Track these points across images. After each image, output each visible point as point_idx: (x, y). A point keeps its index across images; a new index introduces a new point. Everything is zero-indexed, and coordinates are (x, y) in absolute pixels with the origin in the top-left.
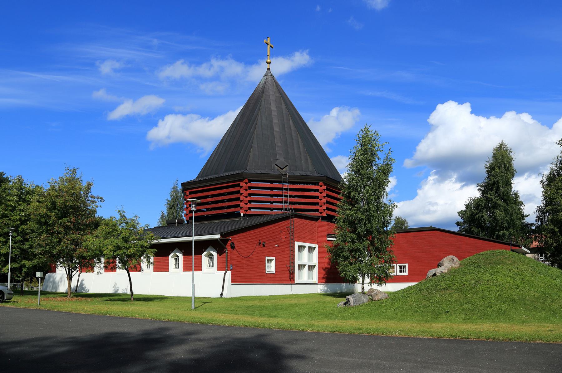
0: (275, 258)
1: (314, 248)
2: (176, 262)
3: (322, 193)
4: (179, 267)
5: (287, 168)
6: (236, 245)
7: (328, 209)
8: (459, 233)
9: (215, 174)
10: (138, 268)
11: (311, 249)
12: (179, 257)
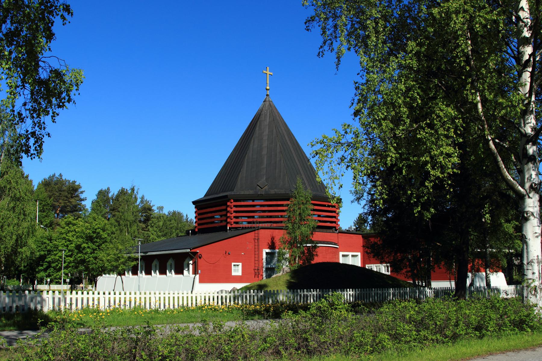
1: (357, 256)
10: (124, 274)
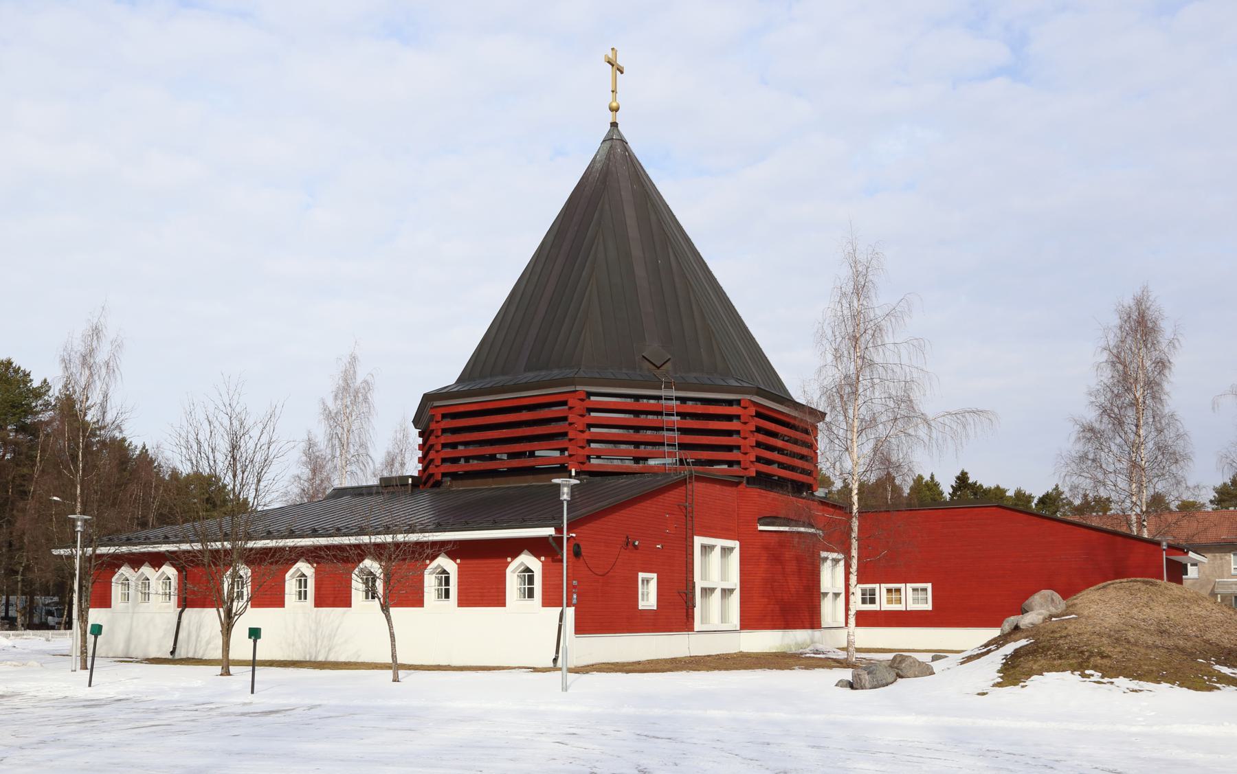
0: (655, 575)
1: (731, 549)
2: (300, 587)
4: (305, 598)
5: (669, 365)
6: (583, 550)
7: (759, 459)
8: (1012, 507)
11: (726, 551)
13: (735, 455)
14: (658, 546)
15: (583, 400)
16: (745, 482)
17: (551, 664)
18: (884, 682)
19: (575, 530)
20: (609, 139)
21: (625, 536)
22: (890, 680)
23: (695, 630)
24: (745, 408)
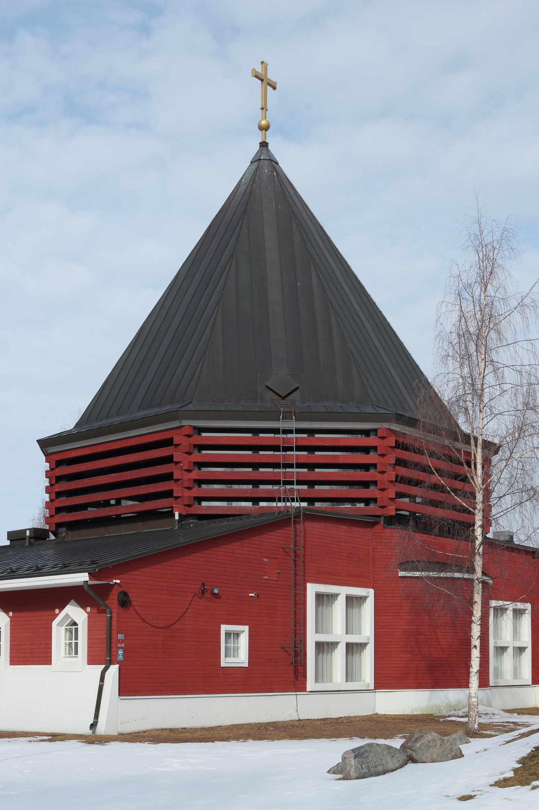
1: (362, 599)
3: (386, 457)
4: (76, 653)
5: (296, 395)
6: (132, 596)
9: (118, 414)
11: (518, 613)
12: (77, 625)
13: (372, 492)
14: (250, 595)
15: (189, 436)
16: (382, 522)
17: (87, 731)
18: (380, 768)
19: (121, 576)
20: (256, 160)
21: (201, 583)
22: (391, 766)
23: (307, 690)
24: (383, 438)
